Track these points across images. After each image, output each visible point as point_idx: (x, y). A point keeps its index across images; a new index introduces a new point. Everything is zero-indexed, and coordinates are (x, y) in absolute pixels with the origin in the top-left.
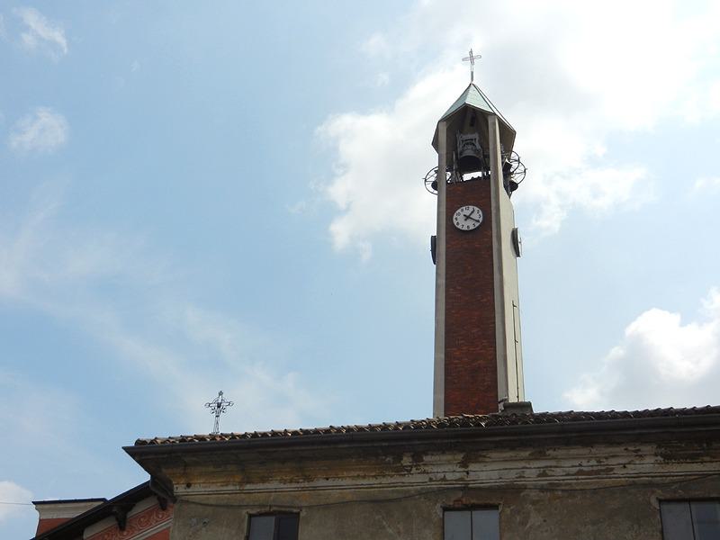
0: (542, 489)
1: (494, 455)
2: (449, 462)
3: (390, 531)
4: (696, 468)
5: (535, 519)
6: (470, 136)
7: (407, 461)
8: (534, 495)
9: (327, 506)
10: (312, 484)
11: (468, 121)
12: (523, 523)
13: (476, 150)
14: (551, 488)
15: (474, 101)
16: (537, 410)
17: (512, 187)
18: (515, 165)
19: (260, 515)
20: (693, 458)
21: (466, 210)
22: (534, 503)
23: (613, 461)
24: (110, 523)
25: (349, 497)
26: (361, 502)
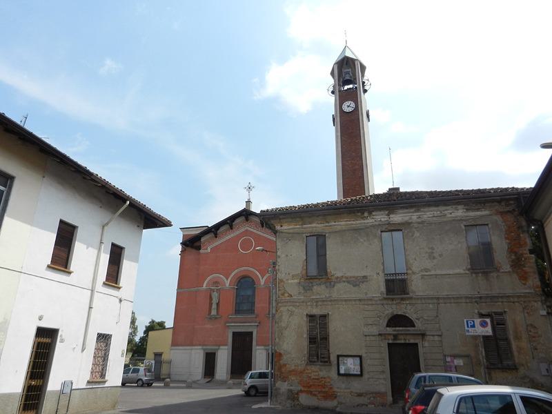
0: (419, 223)
1: (401, 211)
2: (382, 215)
3: (362, 240)
4: (478, 213)
5: (417, 234)
6: (347, 70)
7: (366, 214)
8: (416, 225)
9: (336, 232)
10: (330, 224)
11: (345, 63)
12: (413, 236)
13: (351, 77)
14: (422, 223)
15: (348, 54)
16: (401, 190)
17: (365, 91)
18: (366, 82)
19: (310, 236)
20: (478, 210)
21: (347, 103)
22: (416, 228)
23: (446, 212)
24: (211, 235)
25: (344, 228)
26: (348, 230)
